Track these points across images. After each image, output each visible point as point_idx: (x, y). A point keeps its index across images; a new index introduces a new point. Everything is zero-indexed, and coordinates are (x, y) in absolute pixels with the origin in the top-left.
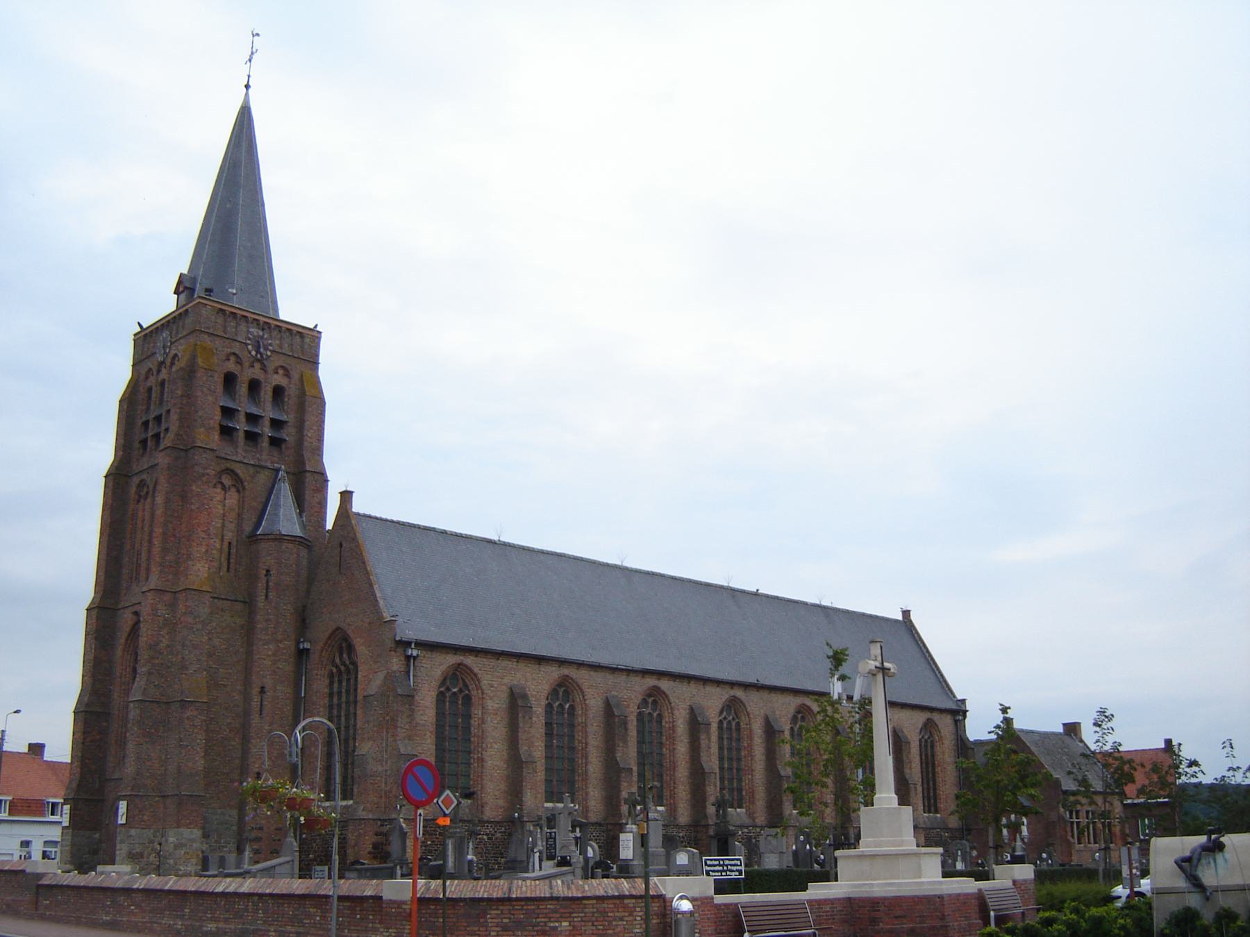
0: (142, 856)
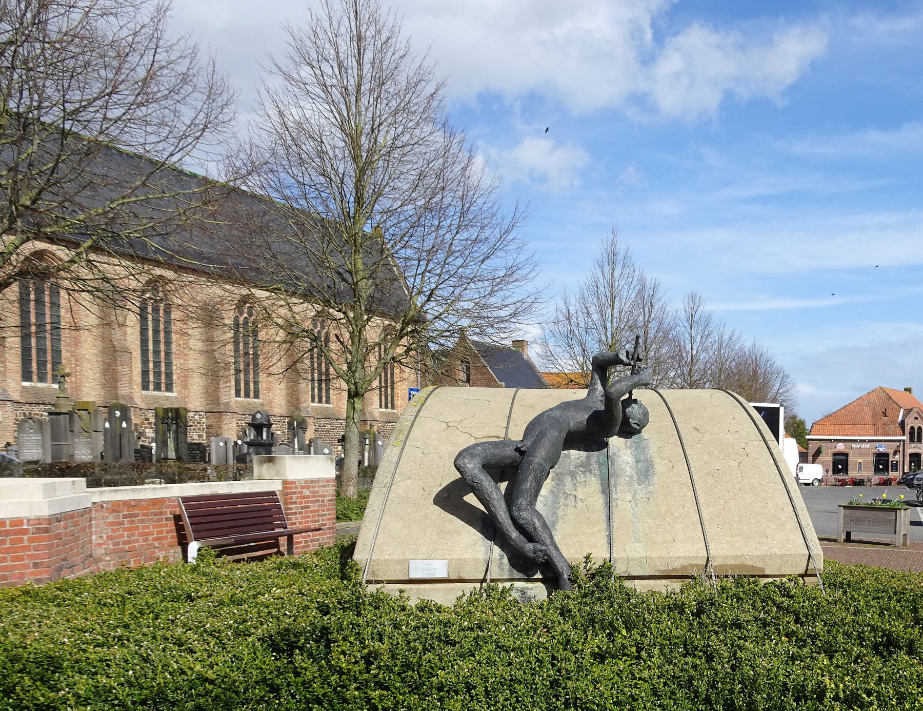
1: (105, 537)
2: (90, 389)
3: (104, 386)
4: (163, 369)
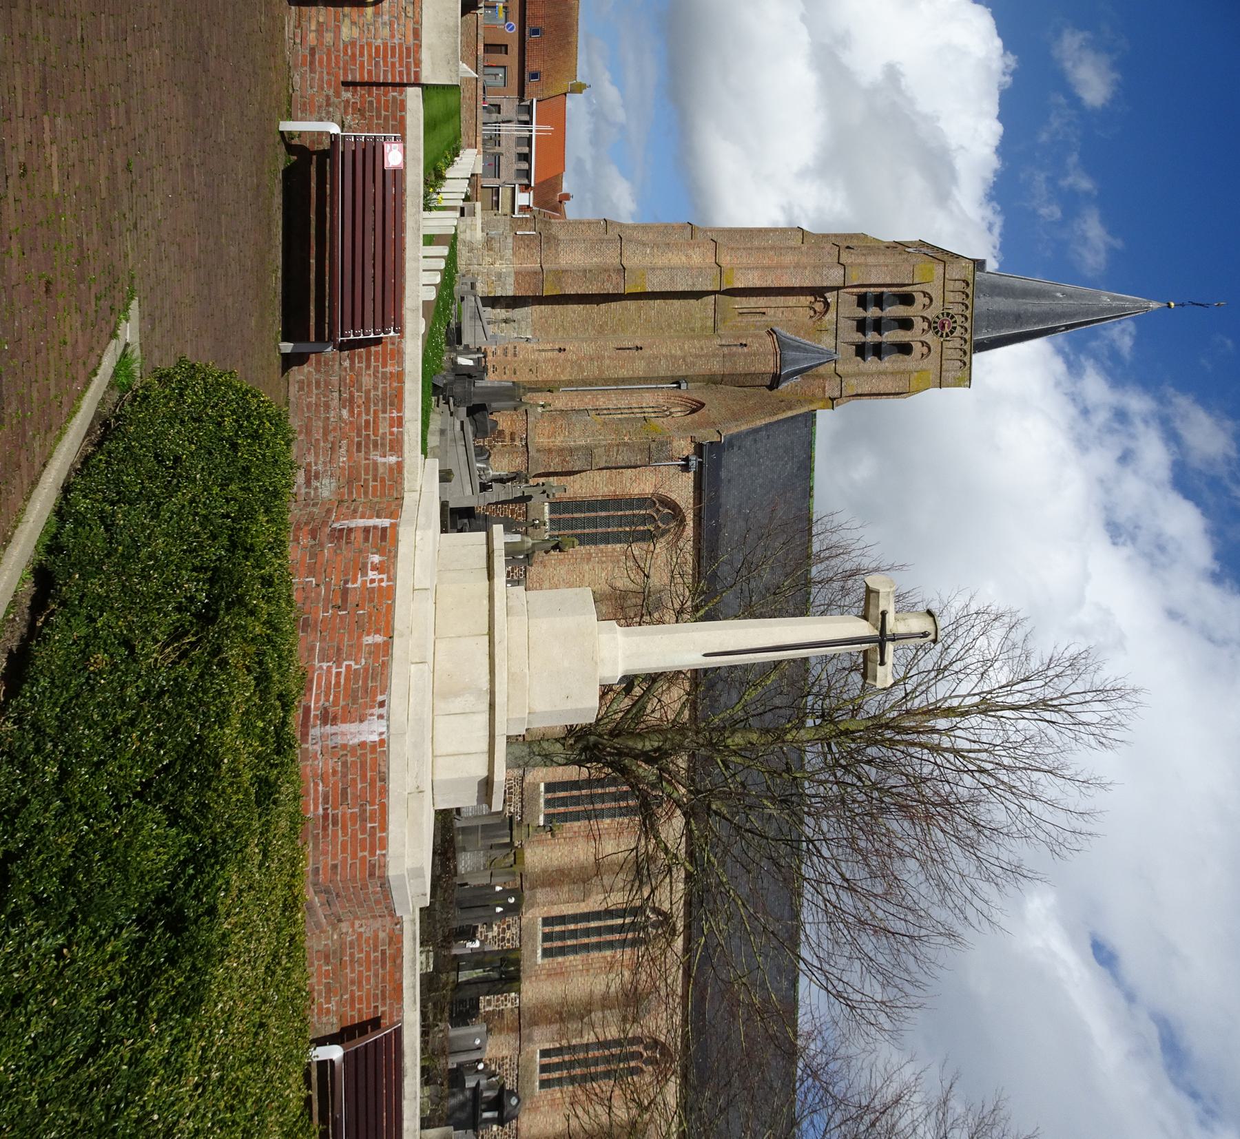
0: (491, 249)
1: (362, 930)
2: (540, 855)
3: (544, 871)
4: (569, 942)
